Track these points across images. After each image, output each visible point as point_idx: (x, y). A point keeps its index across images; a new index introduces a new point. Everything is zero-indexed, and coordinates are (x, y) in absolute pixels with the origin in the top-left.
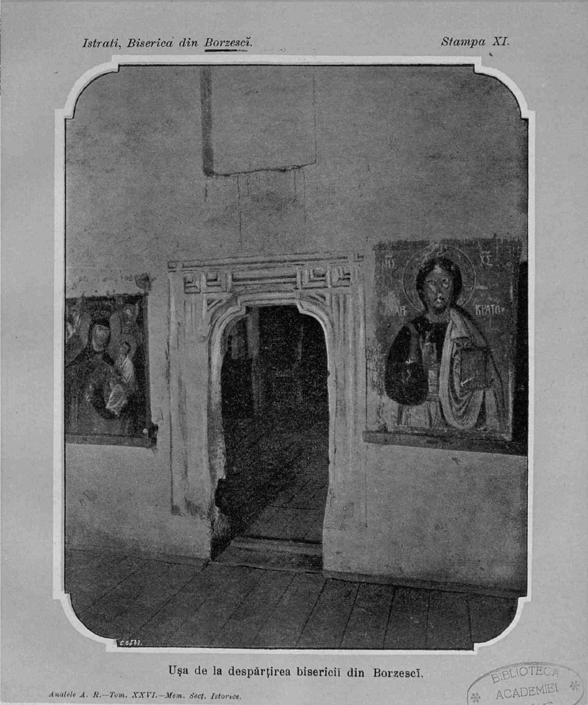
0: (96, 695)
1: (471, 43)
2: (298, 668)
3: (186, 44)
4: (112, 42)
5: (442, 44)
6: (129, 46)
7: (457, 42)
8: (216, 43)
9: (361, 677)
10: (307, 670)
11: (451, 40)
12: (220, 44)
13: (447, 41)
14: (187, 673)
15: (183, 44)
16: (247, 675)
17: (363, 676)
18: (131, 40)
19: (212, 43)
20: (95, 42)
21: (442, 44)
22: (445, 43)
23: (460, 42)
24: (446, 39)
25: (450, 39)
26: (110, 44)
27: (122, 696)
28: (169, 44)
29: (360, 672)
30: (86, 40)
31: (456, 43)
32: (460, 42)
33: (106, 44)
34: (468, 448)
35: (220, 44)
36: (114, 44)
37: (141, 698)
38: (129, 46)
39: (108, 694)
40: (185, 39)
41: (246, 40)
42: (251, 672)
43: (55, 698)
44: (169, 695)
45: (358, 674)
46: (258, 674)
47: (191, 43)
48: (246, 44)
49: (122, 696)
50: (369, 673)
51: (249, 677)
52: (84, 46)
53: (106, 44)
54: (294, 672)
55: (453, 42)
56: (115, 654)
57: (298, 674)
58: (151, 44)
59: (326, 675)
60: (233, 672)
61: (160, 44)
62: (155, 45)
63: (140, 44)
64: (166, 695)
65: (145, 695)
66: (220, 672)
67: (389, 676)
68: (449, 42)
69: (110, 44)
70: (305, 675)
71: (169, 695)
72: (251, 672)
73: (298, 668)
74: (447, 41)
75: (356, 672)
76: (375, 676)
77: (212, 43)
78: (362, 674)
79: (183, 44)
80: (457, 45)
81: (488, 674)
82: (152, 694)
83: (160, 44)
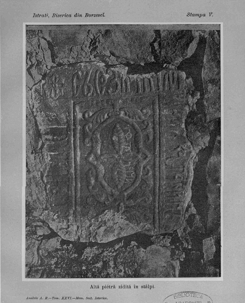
0: (46, 298)
1: (200, 15)
3: (77, 15)
4: (46, 15)
5: (187, 16)
6: (53, 17)
7: (43, 16)
9: (137, 289)
11: (191, 14)
12: (91, 16)
13: (189, 14)
15: (76, 16)
18: (86, 14)
19: (88, 15)
20: (38, 15)
21: (187, 16)
22: (188, 15)
24: (189, 14)
25: (191, 14)
26: (44, 16)
29: (136, 286)
30: (34, 14)
31: (204, 15)
33: (43, 16)
35: (91, 16)
40: (77, 14)
41: (102, 14)
42: (151, 287)
43: (29, 300)
44: (77, 298)
46: (92, 288)
47: (79, 16)
48: (103, 15)
50: (132, 287)
51: (150, 289)
52: (34, 17)
53: (43, 16)
55: (192, 15)
56: (224, 278)
62: (64, 16)
64: (76, 298)
66: (137, 287)
68: (190, 15)
69: (44, 16)
71: (77, 298)
72: (151, 287)
74: (189, 14)
76: (134, 288)
77: (88, 15)
79: (76, 16)
80: (194, 16)
81: (172, 295)
82: (70, 298)
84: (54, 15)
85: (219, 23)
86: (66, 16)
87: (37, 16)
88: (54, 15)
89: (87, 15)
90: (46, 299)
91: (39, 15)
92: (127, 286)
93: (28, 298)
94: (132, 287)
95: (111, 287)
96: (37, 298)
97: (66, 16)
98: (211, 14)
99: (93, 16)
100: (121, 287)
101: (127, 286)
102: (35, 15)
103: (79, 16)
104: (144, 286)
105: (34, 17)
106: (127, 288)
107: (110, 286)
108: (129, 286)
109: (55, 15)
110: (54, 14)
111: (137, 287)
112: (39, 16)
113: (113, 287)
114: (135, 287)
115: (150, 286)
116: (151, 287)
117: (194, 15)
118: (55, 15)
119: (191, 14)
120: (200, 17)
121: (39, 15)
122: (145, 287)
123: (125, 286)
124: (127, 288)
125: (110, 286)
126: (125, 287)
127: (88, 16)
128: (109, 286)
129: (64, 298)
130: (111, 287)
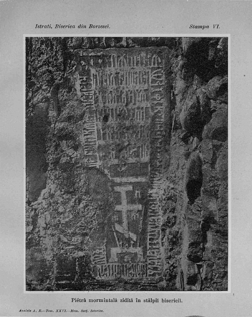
0: (40, 311)
2: (162, 299)
3: (81, 27)
4: (48, 26)
5: (190, 28)
7: (196, 27)
8: (94, 26)
9: (157, 303)
10: (166, 300)
11: (194, 26)
14: (85, 302)
15: (79, 27)
16: (152, 302)
17: (140, 302)
18: (57, 25)
19: (92, 26)
20: (41, 26)
21: (190, 28)
22: (191, 27)
23: (198, 27)
24: (191, 25)
25: (193, 25)
27: (77, 311)
28: (74, 27)
30: (37, 25)
32: (198, 27)
33: (46, 27)
34: (49, 40)
36: (49, 27)
37: (60, 312)
38: (36, 28)
39: (45, 310)
40: (81, 25)
42: (154, 301)
45: (105, 301)
48: (107, 27)
49: (77, 311)
50: (134, 300)
53: (46, 27)
54: (160, 301)
55: (194, 27)
57: (162, 302)
58: (65, 27)
59: (174, 302)
60: (90, 301)
61: (69, 27)
62: (67, 27)
63: (61, 27)
64: (71, 311)
65: (61, 311)
66: (139, 301)
67: (97, 301)
68: (193, 27)
69: (47, 26)
70: (165, 302)
72: (154, 301)
73: (162, 299)
75: (128, 300)
76: (137, 302)
77: (92, 26)
78: (116, 301)
79: (79, 27)
82: (65, 310)
83: (69, 27)
84: (57, 26)
85: (24, 39)
86: (70, 27)
87: (40, 27)
88: (57, 25)
89: (91, 26)
90: (40, 312)
91: (41, 27)
92: (129, 299)
93: (21, 311)
94: (134, 300)
95: (81, 301)
96: (31, 311)
97: (70, 27)
98: (215, 26)
99: (98, 27)
100: (122, 301)
101: (129, 299)
102: (37, 25)
103: (83, 27)
104: (147, 300)
105: (36, 28)
106: (129, 301)
107: (80, 300)
108: (131, 299)
109: (58, 25)
110: (90, 25)
111: (139, 301)
112: (41, 27)
113: (83, 301)
114: (138, 301)
115: (153, 300)
116: (179, 301)
117: (200, 27)
118: (58, 25)
119: (194, 26)
120: (203, 29)
121: (41, 27)
122: (148, 301)
123: (127, 299)
124: (129, 301)
125: (80, 300)
126: (127, 301)
127: (92, 27)
128: (79, 299)
129: (58, 311)
130: (81, 301)
